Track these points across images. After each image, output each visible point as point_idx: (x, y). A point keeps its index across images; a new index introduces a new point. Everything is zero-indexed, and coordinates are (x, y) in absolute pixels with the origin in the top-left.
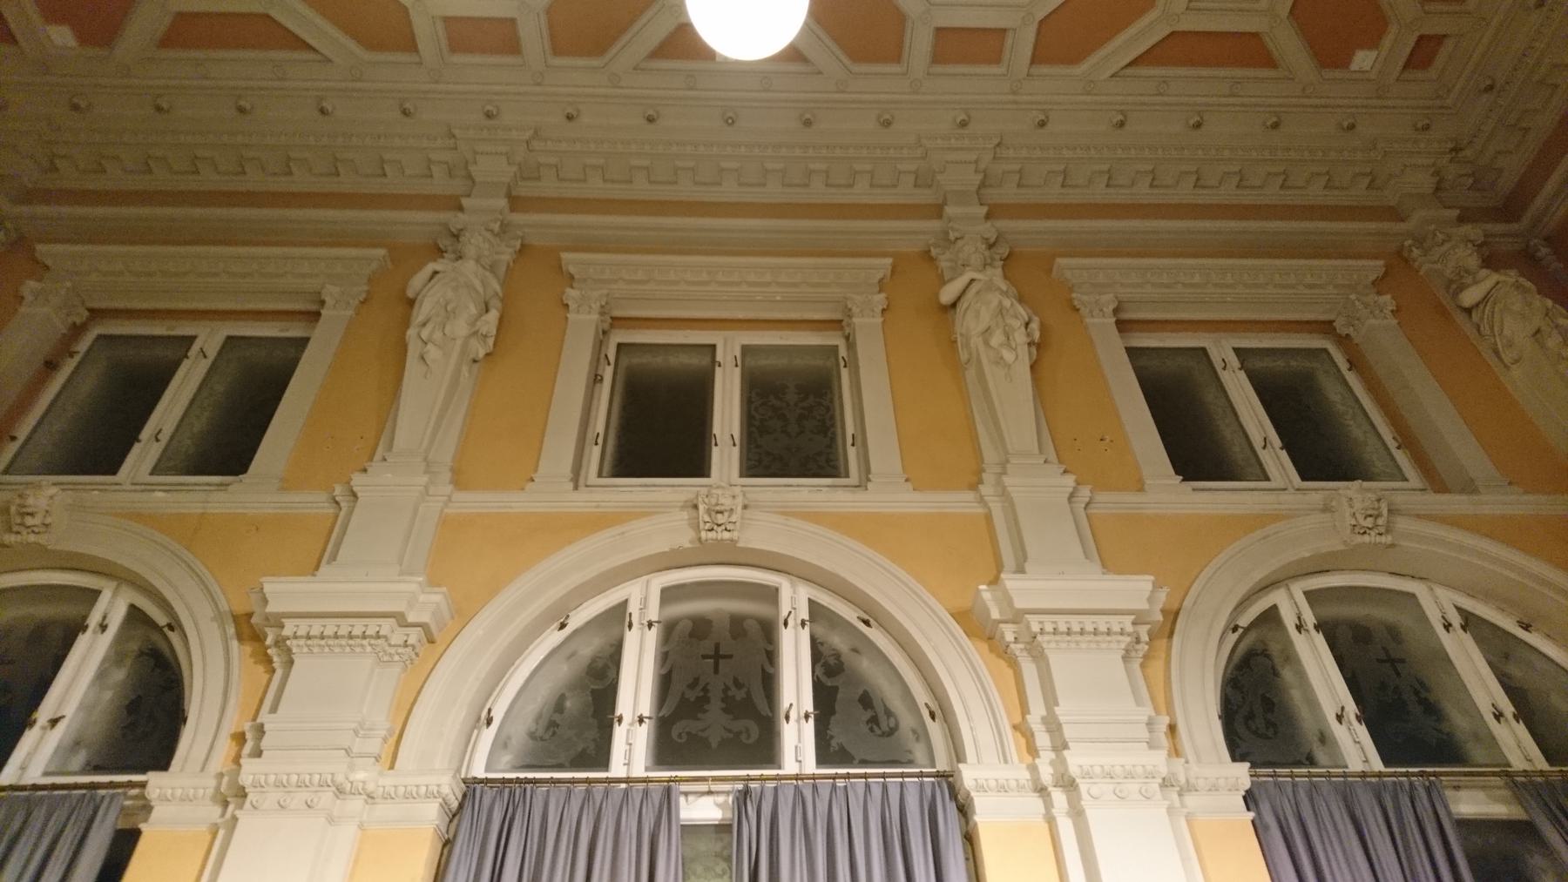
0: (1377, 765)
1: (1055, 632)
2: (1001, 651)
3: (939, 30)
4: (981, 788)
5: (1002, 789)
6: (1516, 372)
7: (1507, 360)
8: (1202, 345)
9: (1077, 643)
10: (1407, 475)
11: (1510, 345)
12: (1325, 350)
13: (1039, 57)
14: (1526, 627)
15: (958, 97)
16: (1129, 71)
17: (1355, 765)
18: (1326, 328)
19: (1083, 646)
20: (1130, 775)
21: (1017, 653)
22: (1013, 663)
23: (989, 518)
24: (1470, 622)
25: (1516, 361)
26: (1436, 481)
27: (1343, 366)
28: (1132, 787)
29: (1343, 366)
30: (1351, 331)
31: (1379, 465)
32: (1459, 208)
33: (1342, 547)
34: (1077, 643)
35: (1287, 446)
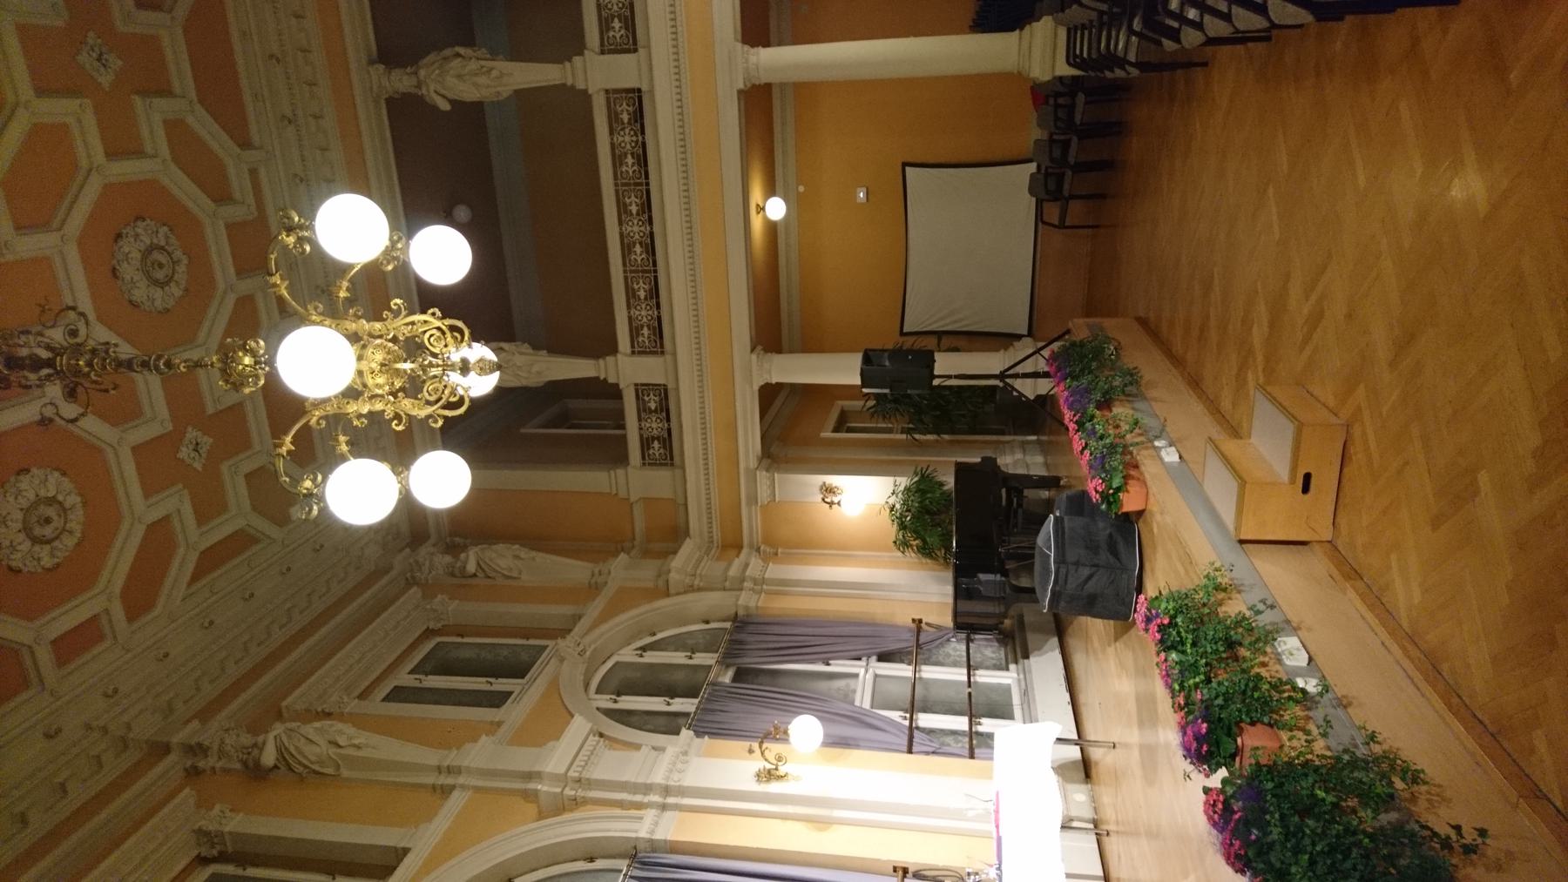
0: (696, 701)
1: (583, 767)
2: (576, 803)
3: (54, 642)
4: (652, 832)
5: (656, 824)
6: (524, 577)
7: (515, 575)
8: (392, 687)
9: (593, 763)
10: (546, 644)
11: (511, 569)
12: (439, 643)
13: (132, 616)
14: (654, 634)
15: (24, 726)
16: (194, 588)
17: (692, 709)
18: (429, 633)
19: (595, 762)
20: (674, 764)
21: (582, 795)
22: (585, 802)
23: (477, 789)
24: (644, 649)
25: (520, 574)
26: (564, 632)
27: (459, 640)
28: (679, 766)
29: (459, 640)
30: (443, 623)
31: (524, 657)
32: (406, 547)
33: (586, 665)
34: (593, 763)
35: (497, 677)
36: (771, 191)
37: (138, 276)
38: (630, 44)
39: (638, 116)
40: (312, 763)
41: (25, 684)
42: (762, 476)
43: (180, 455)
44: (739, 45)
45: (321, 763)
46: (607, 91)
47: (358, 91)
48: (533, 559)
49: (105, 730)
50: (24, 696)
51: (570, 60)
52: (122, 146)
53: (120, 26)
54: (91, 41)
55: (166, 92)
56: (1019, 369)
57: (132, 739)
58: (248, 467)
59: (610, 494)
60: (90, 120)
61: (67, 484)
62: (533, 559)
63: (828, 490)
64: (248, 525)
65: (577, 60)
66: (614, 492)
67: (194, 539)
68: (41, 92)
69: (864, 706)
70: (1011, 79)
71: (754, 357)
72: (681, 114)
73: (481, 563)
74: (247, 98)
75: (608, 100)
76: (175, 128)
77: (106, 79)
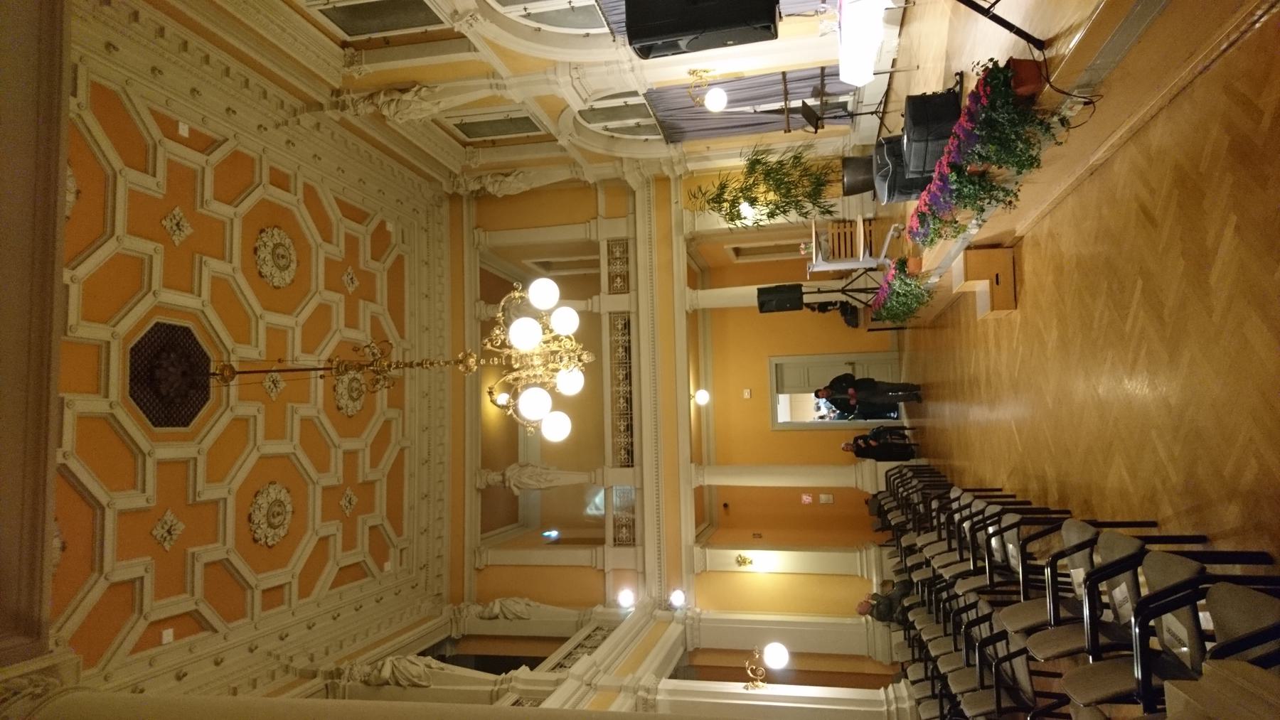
36: (698, 388)
37: (345, 392)
38: (625, 289)
39: (627, 325)
40: (413, 677)
41: (243, 615)
42: (697, 549)
43: (341, 503)
44: (687, 288)
45: (419, 677)
46: (610, 313)
47: (467, 313)
48: (538, 607)
49: (278, 657)
50: (241, 622)
51: (591, 298)
52: (352, 323)
53: (362, 266)
54: (349, 270)
55: (373, 300)
56: (847, 288)
57: (293, 668)
58: (371, 523)
59: (591, 567)
60: (342, 306)
61: (289, 499)
62: (538, 607)
63: (741, 562)
64: (364, 561)
65: (595, 298)
66: (594, 565)
67: (340, 558)
68: (328, 288)
69: (805, 296)
70: (855, 491)
71: (693, 465)
72: (653, 327)
73: (504, 609)
74: (407, 313)
75: (610, 318)
76: (375, 321)
77: (351, 290)
